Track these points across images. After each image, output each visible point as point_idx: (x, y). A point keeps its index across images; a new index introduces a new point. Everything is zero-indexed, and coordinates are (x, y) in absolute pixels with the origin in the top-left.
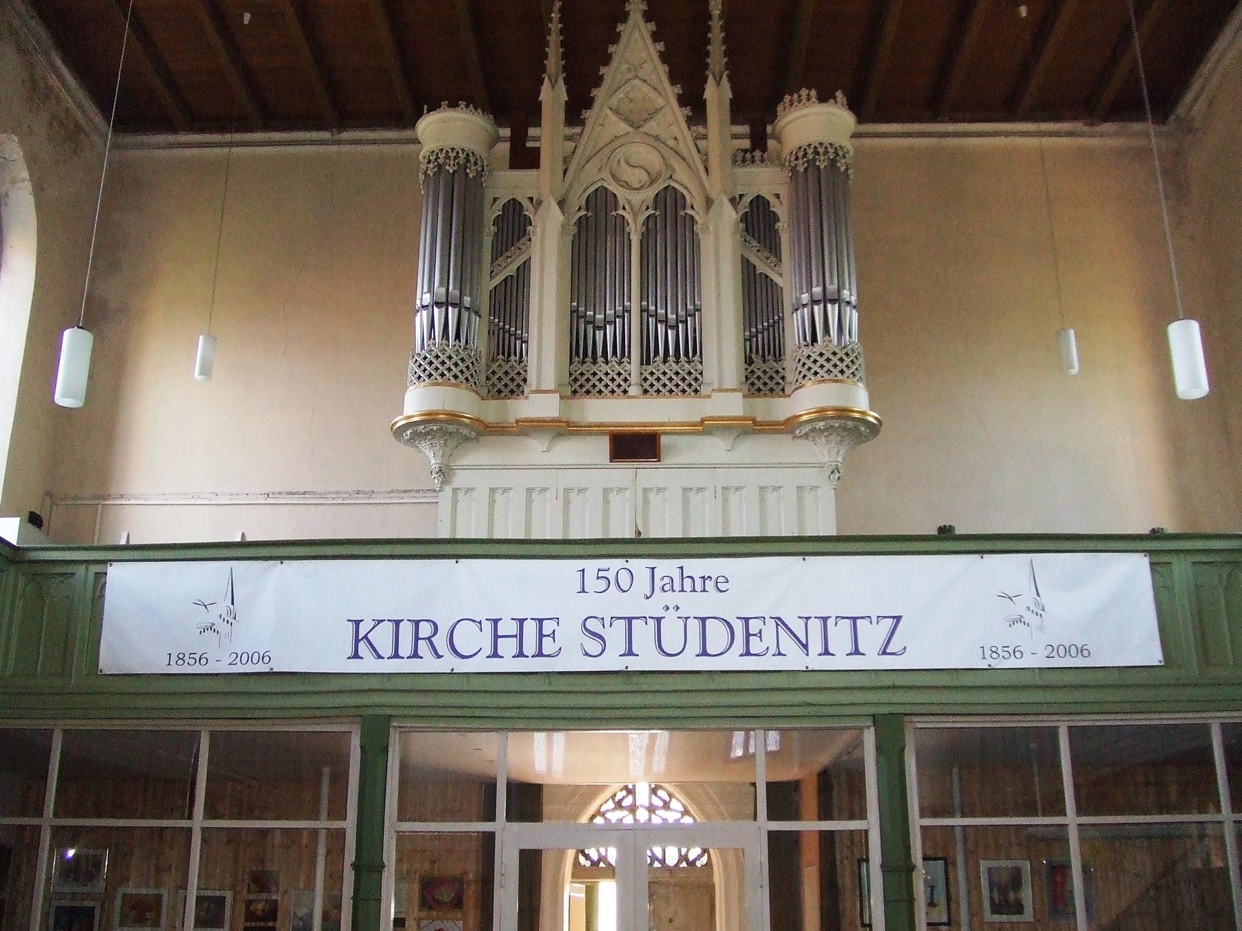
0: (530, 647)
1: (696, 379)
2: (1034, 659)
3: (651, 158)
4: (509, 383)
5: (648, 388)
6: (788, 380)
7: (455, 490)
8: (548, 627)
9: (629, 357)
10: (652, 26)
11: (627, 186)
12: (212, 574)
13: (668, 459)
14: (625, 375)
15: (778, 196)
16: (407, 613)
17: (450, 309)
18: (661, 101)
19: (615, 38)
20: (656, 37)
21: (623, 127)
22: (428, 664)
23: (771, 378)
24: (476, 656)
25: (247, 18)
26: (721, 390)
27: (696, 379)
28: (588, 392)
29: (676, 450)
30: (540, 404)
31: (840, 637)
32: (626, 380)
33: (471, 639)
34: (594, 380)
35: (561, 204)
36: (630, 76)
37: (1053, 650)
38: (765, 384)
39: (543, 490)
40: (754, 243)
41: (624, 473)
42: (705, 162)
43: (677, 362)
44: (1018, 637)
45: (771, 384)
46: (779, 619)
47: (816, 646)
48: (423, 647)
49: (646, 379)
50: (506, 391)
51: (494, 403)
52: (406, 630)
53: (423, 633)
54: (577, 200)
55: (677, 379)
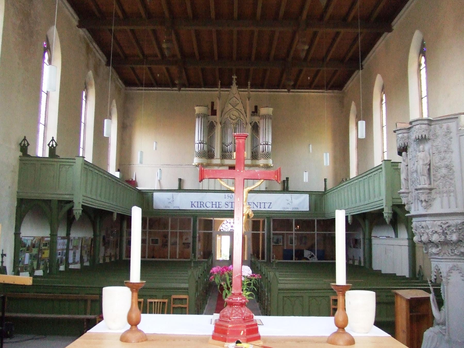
0: (217, 206)
2: (290, 210)
3: (236, 113)
8: (220, 203)
10: (237, 86)
11: (232, 119)
12: (170, 194)
16: (199, 201)
21: (232, 107)
22: (202, 208)
24: (210, 207)
25: (158, 75)
30: (217, 161)
31: (262, 205)
33: (209, 205)
37: (293, 208)
42: (246, 113)
44: (288, 206)
46: (254, 203)
47: (259, 207)
48: (202, 206)
52: (199, 203)
53: (201, 204)
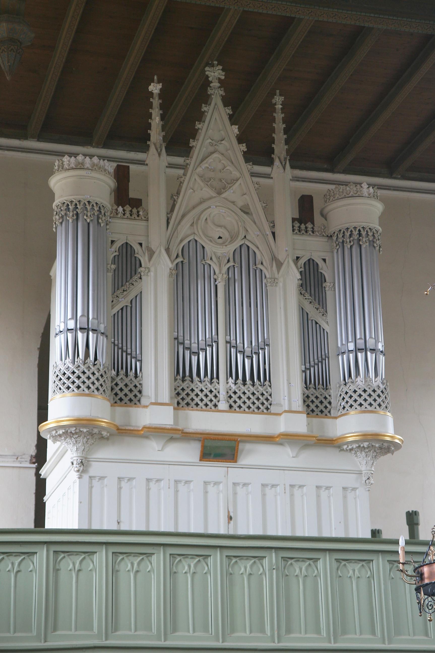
1: (267, 400)
4: (128, 393)
5: (233, 404)
6: (333, 405)
7: (90, 477)
9: (218, 378)
13: (244, 460)
14: (215, 392)
15: (324, 260)
17: (91, 333)
18: (236, 174)
19: (200, 117)
20: (233, 119)
21: (207, 192)
23: (321, 402)
26: (290, 411)
27: (267, 400)
28: (188, 404)
29: (254, 455)
30: (156, 411)
32: (216, 396)
34: (193, 395)
35: (168, 250)
36: (211, 149)
38: (317, 406)
39: (158, 481)
40: (307, 296)
41: (215, 470)
43: (253, 385)
45: (321, 407)
49: (230, 397)
50: (126, 400)
51: (119, 410)
54: (176, 249)
55: (253, 398)
